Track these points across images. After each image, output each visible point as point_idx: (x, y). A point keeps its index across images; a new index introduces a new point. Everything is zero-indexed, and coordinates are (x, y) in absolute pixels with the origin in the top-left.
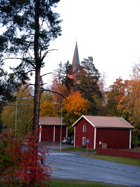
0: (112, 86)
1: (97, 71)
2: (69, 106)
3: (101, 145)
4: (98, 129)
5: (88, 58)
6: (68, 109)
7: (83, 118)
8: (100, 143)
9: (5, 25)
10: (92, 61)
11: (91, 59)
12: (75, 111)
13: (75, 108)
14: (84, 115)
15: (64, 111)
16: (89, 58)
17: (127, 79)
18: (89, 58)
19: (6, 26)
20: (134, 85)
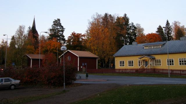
0: (70, 37)
1: (62, 27)
2: (50, 47)
3: (82, 68)
4: (80, 58)
5: (57, 19)
6: (49, 49)
7: (68, 51)
8: (81, 67)
9: (31, 27)
10: (60, 21)
11: (125, 15)
12: (54, 49)
13: (54, 48)
14: (69, 50)
15: (47, 50)
16: (58, 19)
17: (109, 13)
18: (58, 19)
19: (116, 18)
20: (126, 44)
